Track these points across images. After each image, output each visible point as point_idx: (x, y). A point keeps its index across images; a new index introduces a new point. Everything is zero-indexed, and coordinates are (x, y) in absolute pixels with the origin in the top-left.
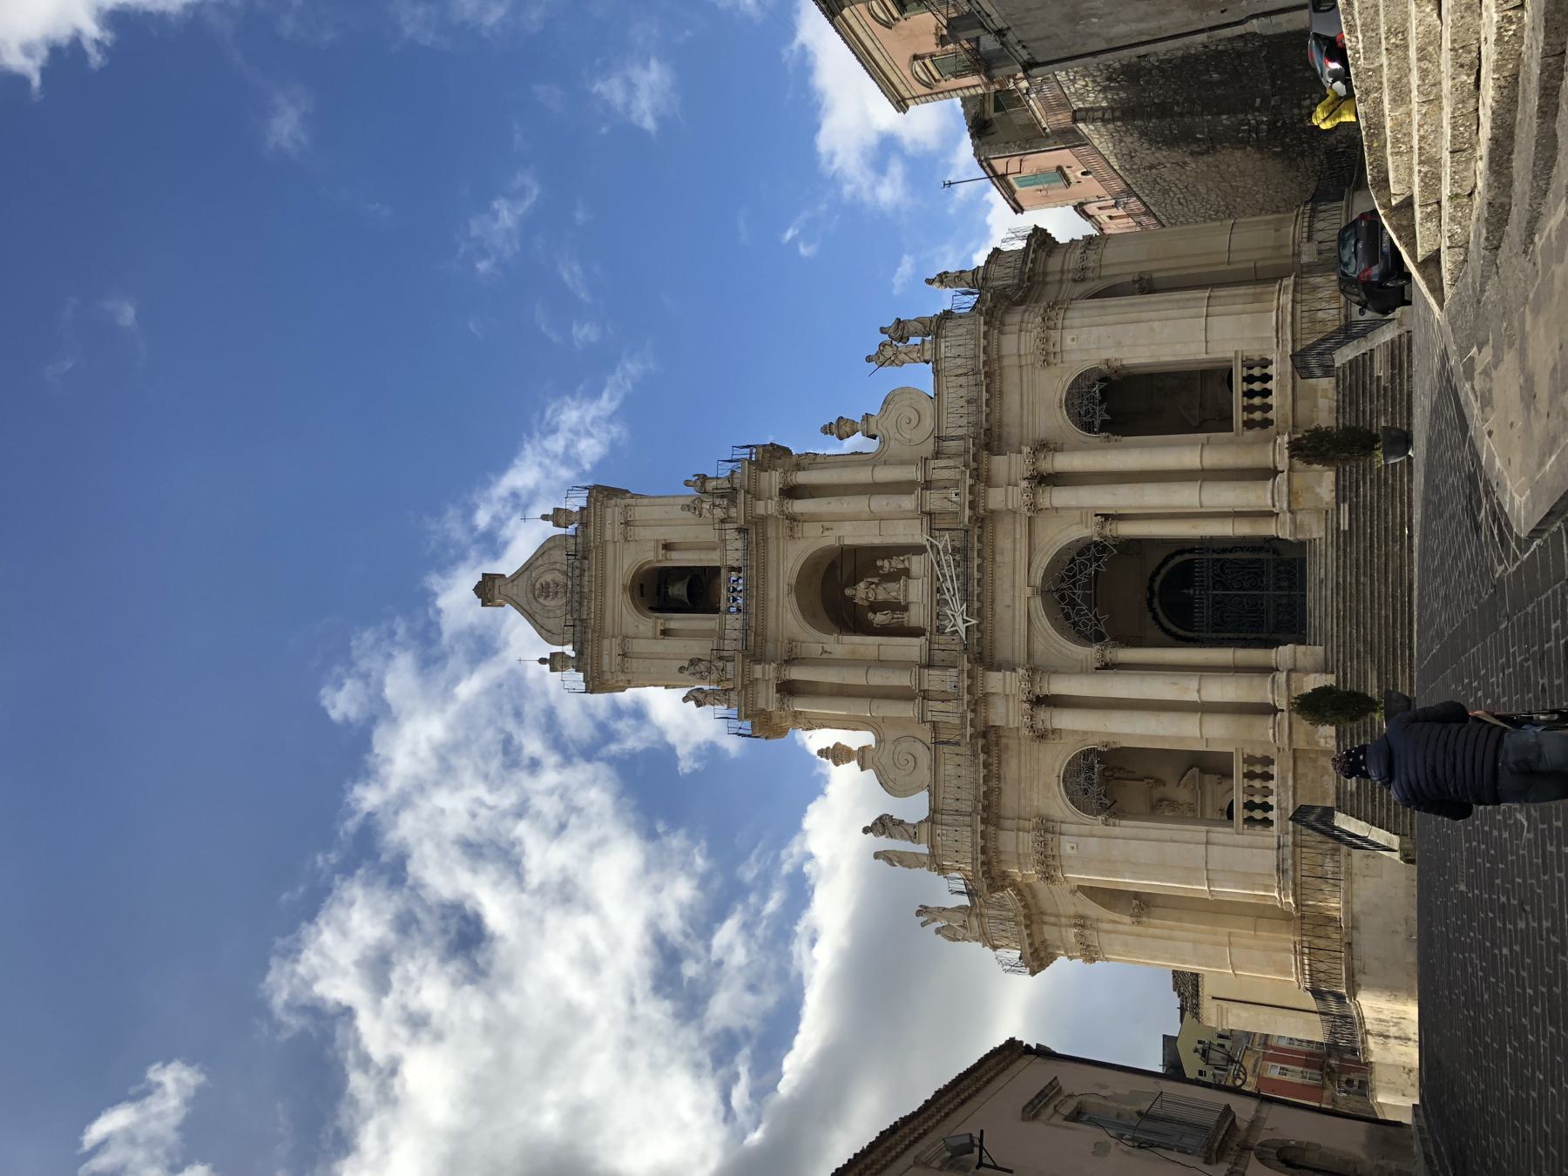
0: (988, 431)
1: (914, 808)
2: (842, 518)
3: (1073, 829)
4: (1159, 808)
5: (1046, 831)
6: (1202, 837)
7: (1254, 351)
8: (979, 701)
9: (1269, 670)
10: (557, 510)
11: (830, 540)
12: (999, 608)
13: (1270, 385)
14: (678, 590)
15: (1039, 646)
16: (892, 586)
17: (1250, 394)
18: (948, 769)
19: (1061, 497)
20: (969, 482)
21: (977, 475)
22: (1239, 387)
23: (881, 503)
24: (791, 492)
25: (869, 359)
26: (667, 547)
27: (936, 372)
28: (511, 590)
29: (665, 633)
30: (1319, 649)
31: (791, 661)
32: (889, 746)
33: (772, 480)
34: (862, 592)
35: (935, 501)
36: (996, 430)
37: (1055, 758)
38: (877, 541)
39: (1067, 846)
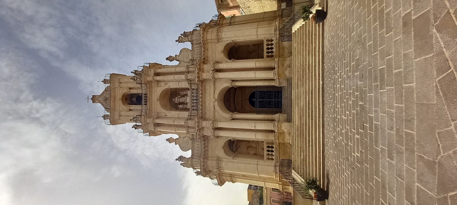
0: (204, 59)
1: (188, 154)
2: (169, 81)
3: (225, 160)
4: (247, 154)
5: (219, 161)
6: (256, 163)
7: (269, 37)
8: (201, 129)
9: (273, 120)
10: (105, 80)
11: (167, 87)
12: (207, 104)
13: (273, 46)
14: (134, 99)
15: (216, 114)
16: (183, 98)
17: (268, 45)
18: (196, 145)
19: (221, 75)
20: (197, 71)
21: (200, 69)
22: (265, 47)
23: (177, 77)
24: (158, 74)
25: (176, 41)
26: (130, 88)
27: (192, 44)
28: (100, 99)
29: (130, 110)
30: (285, 115)
31: (158, 118)
32: (182, 139)
33: (152, 72)
34: (176, 100)
35: (190, 76)
36: (206, 58)
37: (221, 143)
38: (178, 87)
39: (223, 164)
